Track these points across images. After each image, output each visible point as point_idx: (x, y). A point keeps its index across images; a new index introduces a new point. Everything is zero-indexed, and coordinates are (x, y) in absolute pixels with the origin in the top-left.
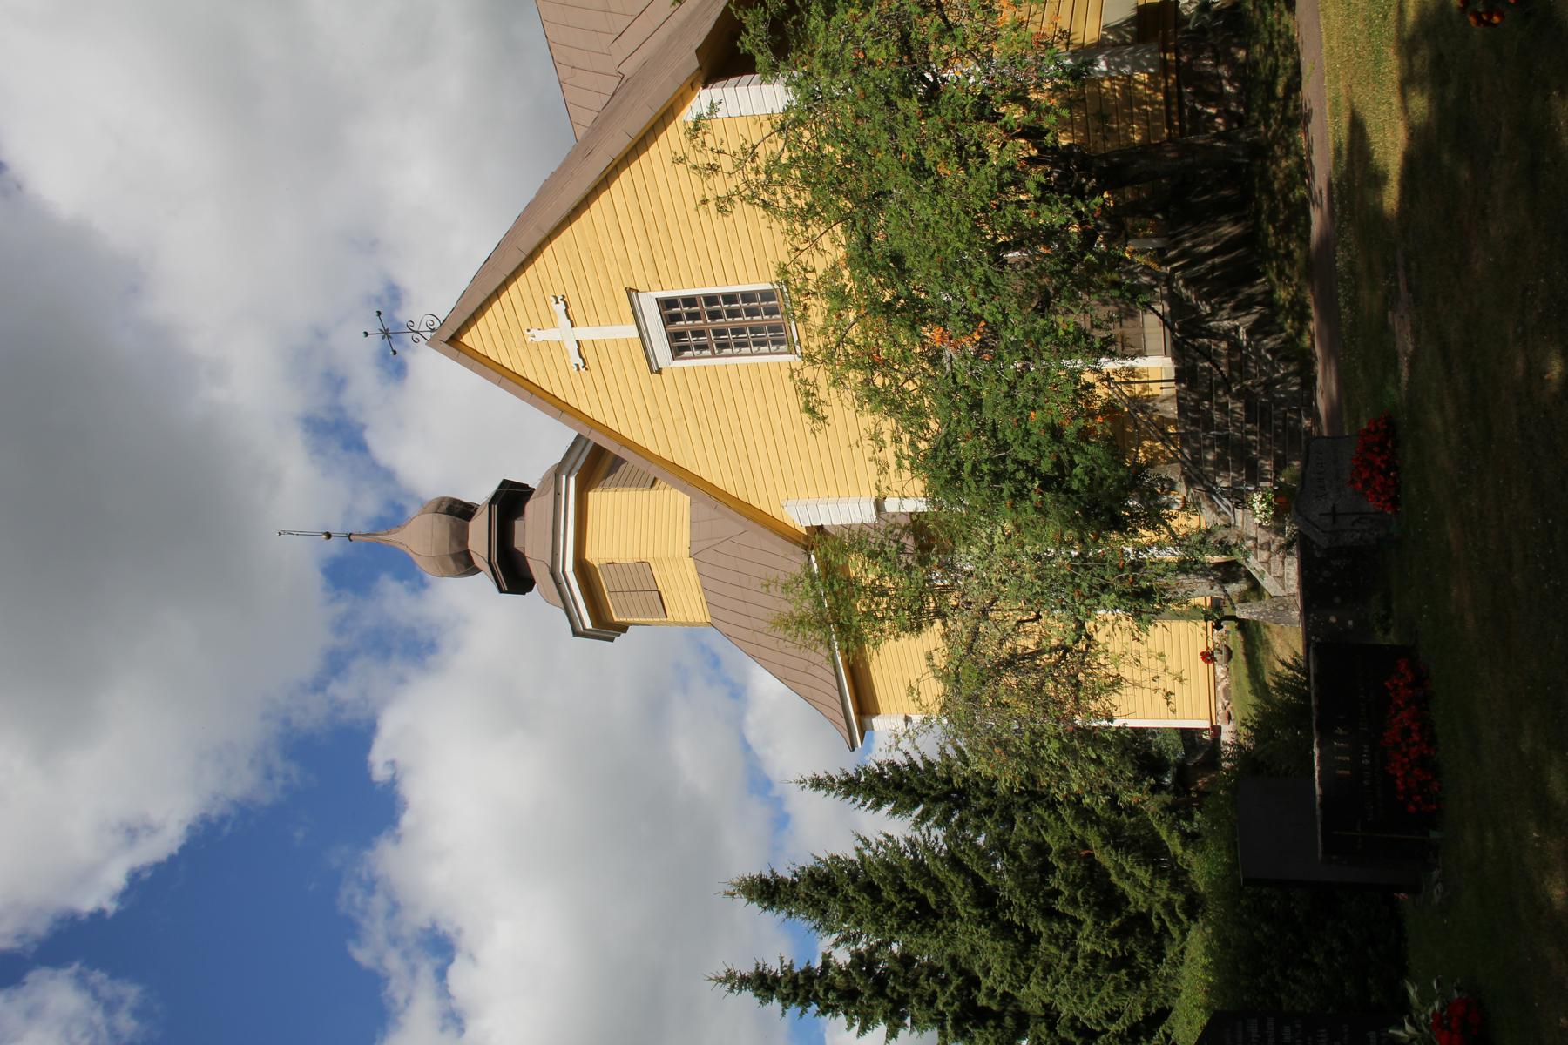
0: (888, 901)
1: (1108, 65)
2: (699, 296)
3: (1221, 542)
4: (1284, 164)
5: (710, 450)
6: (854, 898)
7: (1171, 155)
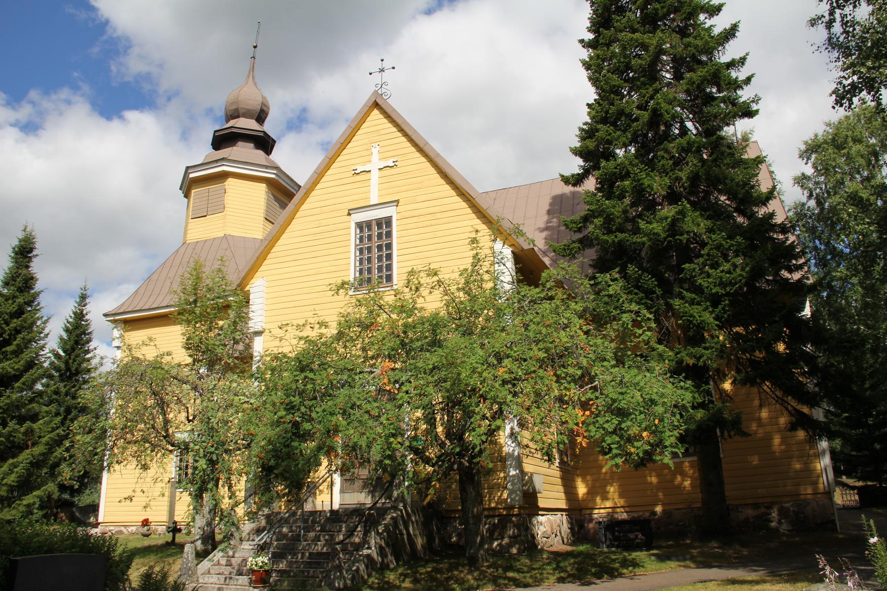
0: (10, 322)
1: (513, 476)
2: (392, 240)
3: (232, 535)
4: (470, 577)
5: (299, 239)
6: (15, 302)
7: (475, 510)
